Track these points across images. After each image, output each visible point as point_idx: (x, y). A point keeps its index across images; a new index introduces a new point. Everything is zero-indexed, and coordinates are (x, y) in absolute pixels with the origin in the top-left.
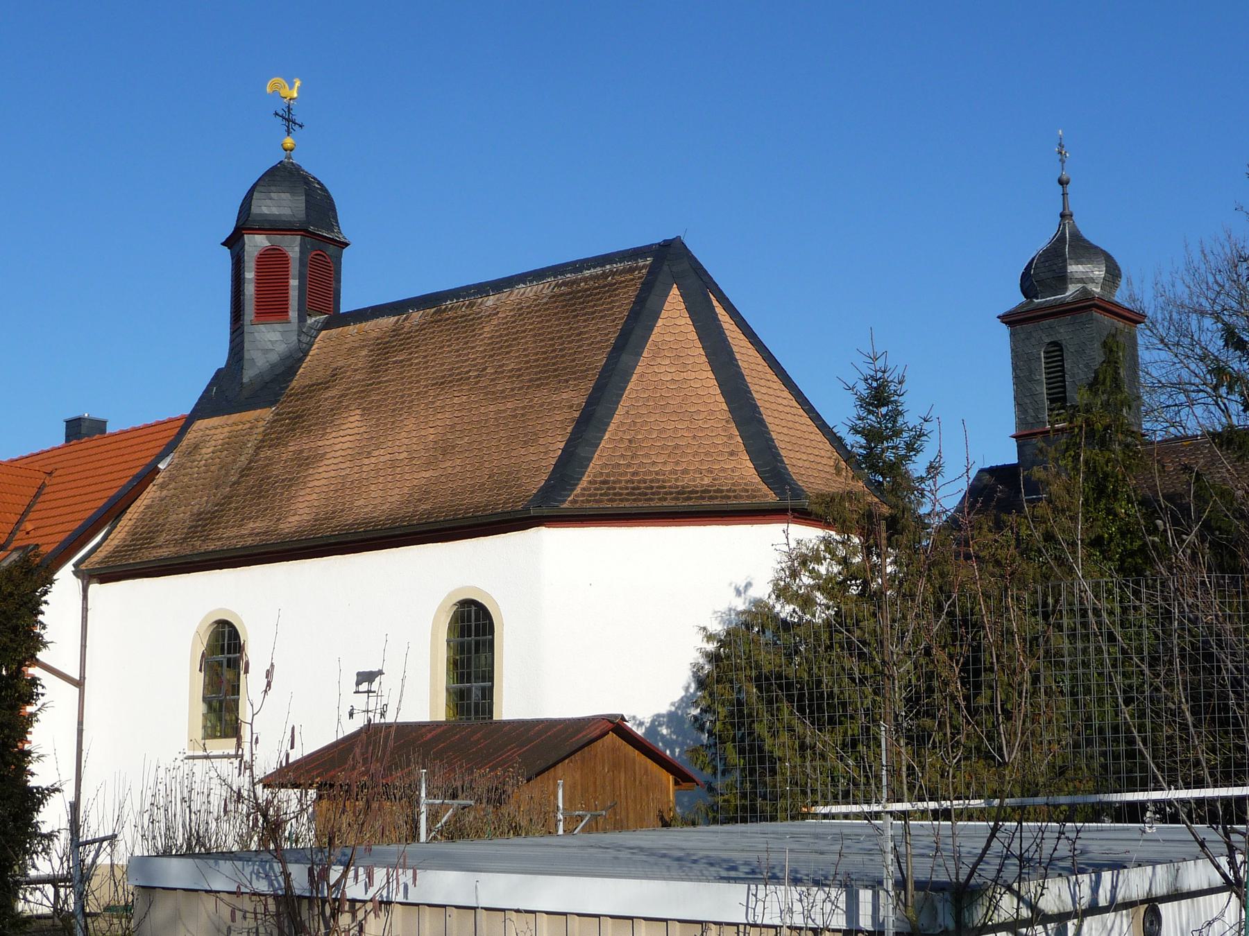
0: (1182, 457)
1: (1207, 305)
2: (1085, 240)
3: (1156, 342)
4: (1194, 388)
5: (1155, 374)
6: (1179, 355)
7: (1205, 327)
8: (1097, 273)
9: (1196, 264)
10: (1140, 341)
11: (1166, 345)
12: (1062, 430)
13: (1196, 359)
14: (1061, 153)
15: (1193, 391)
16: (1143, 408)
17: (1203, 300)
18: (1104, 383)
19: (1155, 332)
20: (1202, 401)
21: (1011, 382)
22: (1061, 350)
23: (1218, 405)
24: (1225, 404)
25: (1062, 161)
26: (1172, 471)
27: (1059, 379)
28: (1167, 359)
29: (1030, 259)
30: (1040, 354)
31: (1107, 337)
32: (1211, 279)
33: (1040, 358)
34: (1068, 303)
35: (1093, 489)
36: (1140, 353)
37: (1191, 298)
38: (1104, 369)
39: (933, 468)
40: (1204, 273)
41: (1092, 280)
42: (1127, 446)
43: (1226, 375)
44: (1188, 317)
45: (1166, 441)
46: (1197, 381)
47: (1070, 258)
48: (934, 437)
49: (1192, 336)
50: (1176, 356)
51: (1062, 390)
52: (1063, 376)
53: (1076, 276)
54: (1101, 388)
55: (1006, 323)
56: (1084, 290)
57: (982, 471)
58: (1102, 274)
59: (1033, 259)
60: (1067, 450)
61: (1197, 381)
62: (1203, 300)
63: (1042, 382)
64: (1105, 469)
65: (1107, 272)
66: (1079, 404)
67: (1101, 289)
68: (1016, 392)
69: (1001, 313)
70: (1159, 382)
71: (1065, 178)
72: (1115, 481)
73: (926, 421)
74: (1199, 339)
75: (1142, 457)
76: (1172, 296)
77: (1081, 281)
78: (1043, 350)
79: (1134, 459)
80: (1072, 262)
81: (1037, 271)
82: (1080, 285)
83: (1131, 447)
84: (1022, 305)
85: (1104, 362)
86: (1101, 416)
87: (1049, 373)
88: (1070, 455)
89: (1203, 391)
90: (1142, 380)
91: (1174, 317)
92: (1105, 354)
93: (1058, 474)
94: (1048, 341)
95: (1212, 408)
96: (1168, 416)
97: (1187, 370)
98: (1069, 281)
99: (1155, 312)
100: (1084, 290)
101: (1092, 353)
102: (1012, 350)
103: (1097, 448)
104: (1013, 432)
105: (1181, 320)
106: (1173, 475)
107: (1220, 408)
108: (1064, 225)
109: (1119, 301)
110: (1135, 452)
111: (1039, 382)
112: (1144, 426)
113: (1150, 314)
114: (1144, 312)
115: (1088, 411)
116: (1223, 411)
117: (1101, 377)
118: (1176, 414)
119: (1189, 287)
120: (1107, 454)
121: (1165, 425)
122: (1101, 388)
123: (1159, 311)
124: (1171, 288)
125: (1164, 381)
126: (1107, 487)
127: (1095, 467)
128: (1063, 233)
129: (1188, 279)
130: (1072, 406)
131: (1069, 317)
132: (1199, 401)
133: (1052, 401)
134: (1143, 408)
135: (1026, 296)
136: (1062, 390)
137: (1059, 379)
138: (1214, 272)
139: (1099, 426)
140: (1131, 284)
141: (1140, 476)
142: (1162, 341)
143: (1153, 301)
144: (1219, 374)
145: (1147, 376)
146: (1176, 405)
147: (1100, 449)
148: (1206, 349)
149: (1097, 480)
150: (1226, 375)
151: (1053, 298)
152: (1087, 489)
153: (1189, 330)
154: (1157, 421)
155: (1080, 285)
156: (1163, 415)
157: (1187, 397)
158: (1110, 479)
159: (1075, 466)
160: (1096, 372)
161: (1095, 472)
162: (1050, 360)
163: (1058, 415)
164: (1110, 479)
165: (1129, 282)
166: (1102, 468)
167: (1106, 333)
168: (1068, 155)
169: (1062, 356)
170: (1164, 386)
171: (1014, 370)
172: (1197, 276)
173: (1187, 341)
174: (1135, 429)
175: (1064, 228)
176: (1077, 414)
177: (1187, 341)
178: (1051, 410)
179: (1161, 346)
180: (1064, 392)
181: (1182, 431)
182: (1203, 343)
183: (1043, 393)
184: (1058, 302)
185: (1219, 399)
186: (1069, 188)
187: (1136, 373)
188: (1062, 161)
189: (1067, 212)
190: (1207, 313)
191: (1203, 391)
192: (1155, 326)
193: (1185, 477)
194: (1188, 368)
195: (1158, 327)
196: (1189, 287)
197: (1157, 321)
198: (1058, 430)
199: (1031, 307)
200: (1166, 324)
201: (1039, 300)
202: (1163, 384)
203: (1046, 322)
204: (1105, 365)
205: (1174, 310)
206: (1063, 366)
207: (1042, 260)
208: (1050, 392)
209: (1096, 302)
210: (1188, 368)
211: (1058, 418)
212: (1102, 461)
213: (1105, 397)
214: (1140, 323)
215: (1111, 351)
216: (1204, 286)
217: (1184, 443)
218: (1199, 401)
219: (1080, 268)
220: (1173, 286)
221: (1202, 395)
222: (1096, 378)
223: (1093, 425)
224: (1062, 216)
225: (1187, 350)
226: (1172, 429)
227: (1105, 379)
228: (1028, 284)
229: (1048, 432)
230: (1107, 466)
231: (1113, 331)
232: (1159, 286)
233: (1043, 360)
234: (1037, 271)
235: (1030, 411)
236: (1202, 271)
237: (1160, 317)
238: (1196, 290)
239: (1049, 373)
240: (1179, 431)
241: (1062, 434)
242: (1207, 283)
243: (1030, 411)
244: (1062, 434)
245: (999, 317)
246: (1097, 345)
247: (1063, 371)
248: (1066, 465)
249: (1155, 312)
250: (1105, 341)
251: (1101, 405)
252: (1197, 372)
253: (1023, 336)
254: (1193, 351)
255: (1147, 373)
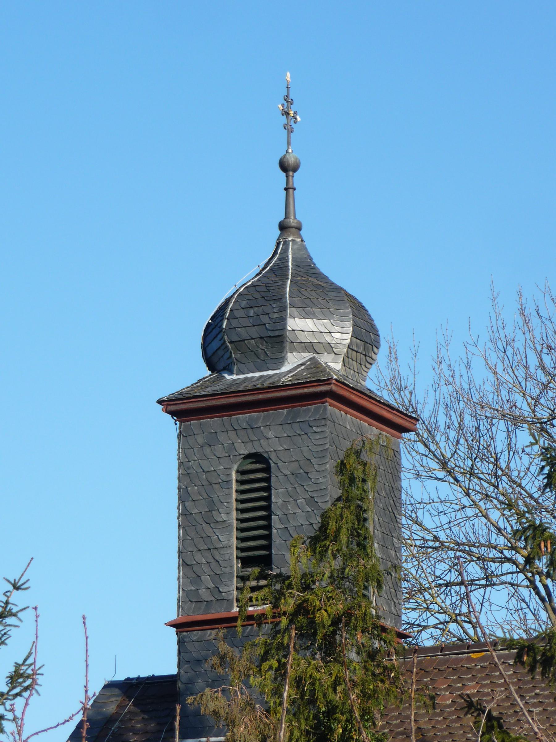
0: (469, 680)
1: (525, 407)
2: (319, 275)
3: (434, 465)
4: (493, 553)
5: (428, 523)
6: (472, 494)
7: (519, 446)
8: (338, 336)
9: (509, 331)
10: (406, 461)
11: (450, 473)
12: (260, 619)
13: (501, 503)
14: (287, 114)
15: (493, 561)
16: (405, 584)
17: (518, 398)
18: (336, 538)
19: (433, 447)
20: (508, 578)
21: (175, 523)
22: (268, 470)
23: (536, 588)
24: (546, 587)
25: (289, 129)
26: (449, 706)
27: (261, 523)
28: (452, 498)
29: (222, 300)
30: (229, 475)
31: (348, 455)
32: (533, 362)
33: (229, 482)
34: (285, 386)
35: (308, 733)
36: (404, 484)
37: (498, 391)
38: (338, 512)
39: (21, 676)
40: (522, 350)
41: (329, 348)
42: (373, 655)
43: (545, 541)
44: (492, 425)
45: (442, 649)
46: (501, 541)
47: (292, 305)
48: (27, 616)
49: (497, 459)
50: (468, 494)
51: (264, 513)
52: (268, 518)
53: (302, 338)
54: (333, 548)
55: (173, 413)
56: (314, 363)
57: (110, 686)
58: (347, 338)
59: (227, 302)
60: (264, 658)
61: (501, 541)
62: (518, 398)
63: (230, 525)
64: (331, 696)
65: (355, 335)
66: (292, 574)
67: (344, 364)
68: (182, 540)
69: (165, 394)
70: (436, 539)
71: (291, 159)
72: (347, 720)
73: (16, 587)
74: (508, 467)
75: (396, 678)
76: (466, 386)
77: (309, 347)
78: (235, 467)
79: (382, 681)
80: (295, 311)
81: (234, 323)
82: (307, 356)
83: (379, 658)
84: (203, 383)
85: (339, 499)
86: (328, 599)
87: (243, 511)
88: (271, 667)
89: (509, 560)
90: (406, 534)
91: (466, 422)
92: (342, 484)
93: (249, 704)
94: (245, 451)
95: (525, 592)
96: (448, 602)
97: (484, 520)
98: (288, 345)
99: (435, 413)
100: (314, 363)
101: (321, 480)
102: (181, 464)
103: (318, 656)
104: (173, 616)
105: (478, 429)
106: (451, 713)
107: (538, 593)
108: (286, 243)
109: (373, 388)
110: (385, 668)
111: (225, 525)
112: (404, 618)
113: (425, 415)
114: (415, 411)
115: (306, 588)
116: (542, 599)
117: (333, 526)
118: (462, 600)
119: (495, 373)
120: (336, 668)
121: (442, 617)
122: (333, 548)
123: (442, 410)
124: (464, 371)
125: (443, 538)
126: (332, 731)
127: (313, 692)
128: (284, 259)
129: (493, 358)
130: (279, 575)
131: (285, 411)
132: (504, 578)
133: (246, 562)
134: (405, 584)
135: (211, 366)
136: (264, 513)
137: (261, 523)
138: (539, 348)
139: (323, 617)
140: (396, 358)
141: (393, 710)
142: (444, 464)
143: (431, 392)
144: (534, 538)
145: (415, 527)
146: (462, 583)
147: (323, 659)
148: (520, 485)
149: (316, 717)
150: (545, 541)
151: (258, 374)
152: (296, 733)
153: (492, 449)
154: (428, 609)
155: (307, 356)
156: (439, 600)
157: (484, 569)
158: (338, 715)
159: (277, 689)
160: (325, 516)
161: (312, 701)
162: (246, 487)
163: (253, 589)
164: (338, 715)
165: (393, 356)
166: (325, 695)
167: (347, 444)
168: (299, 119)
169: (268, 480)
170: (442, 546)
171: (182, 500)
172: (509, 352)
173: (485, 468)
174: (388, 623)
175: (285, 250)
176: (287, 592)
177: (485, 468)
178: (243, 579)
179: (441, 474)
180: (268, 547)
181: (471, 632)
182: (515, 474)
183: (229, 547)
184: (267, 384)
185: (537, 577)
186: (298, 178)
187: (395, 520)
188: (289, 129)
189: (292, 221)
190: (524, 421)
191: (509, 560)
192: (433, 437)
193: (469, 720)
194: (486, 517)
195: (438, 438)
196: (495, 373)
197: (437, 428)
198: (250, 617)
199: (219, 387)
200: (452, 434)
201: (234, 377)
202: (442, 543)
203: (243, 417)
204: (340, 504)
205: (468, 411)
206: (268, 499)
207: (244, 304)
208: (244, 545)
209: (333, 387)
210: (486, 517)
211: (254, 595)
212: (327, 681)
213: (337, 564)
214: (407, 430)
215: (352, 480)
216: (521, 373)
217: (473, 656)
218: (504, 578)
219: (308, 324)
220: (468, 366)
221: (507, 567)
222: (323, 528)
223: (314, 613)
224: (283, 227)
225: (486, 485)
226: (453, 627)
227: (338, 531)
228: (215, 345)
229: (234, 619)
230: (335, 691)
231: (357, 446)
232: (444, 366)
233: (234, 486)
234: (234, 323)
235: (206, 578)
236: (519, 344)
237: (442, 420)
238: (507, 377)
239: (243, 511)
240: (465, 632)
241: (259, 625)
242: (526, 367)
243: (206, 578)
244: (259, 625)
245: (160, 402)
246: (330, 465)
247: (268, 508)
248: (262, 686)
249: (435, 413)
250: (342, 462)
251: (331, 577)
252: (501, 525)
253: (200, 440)
254: (497, 487)
255: (416, 523)
